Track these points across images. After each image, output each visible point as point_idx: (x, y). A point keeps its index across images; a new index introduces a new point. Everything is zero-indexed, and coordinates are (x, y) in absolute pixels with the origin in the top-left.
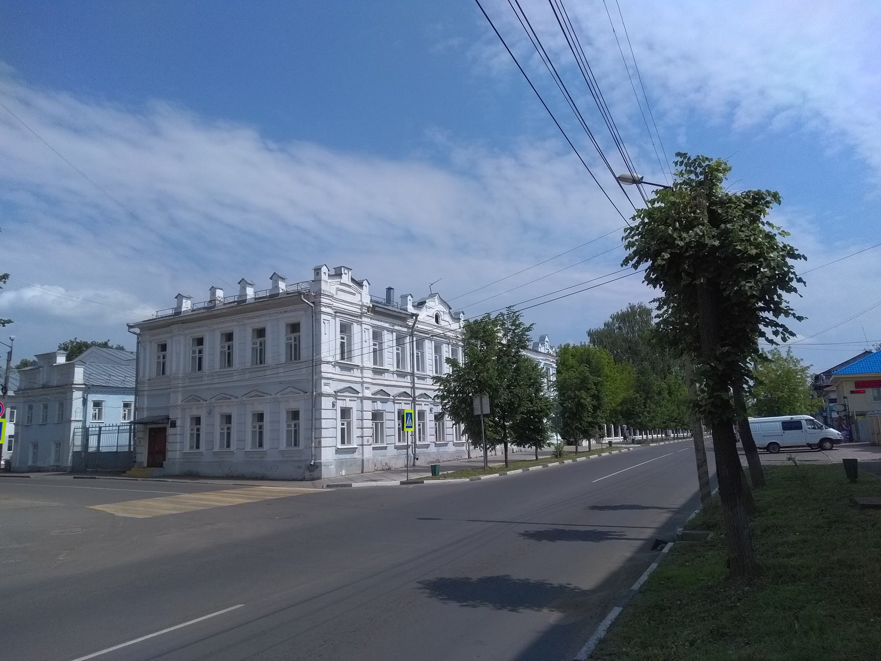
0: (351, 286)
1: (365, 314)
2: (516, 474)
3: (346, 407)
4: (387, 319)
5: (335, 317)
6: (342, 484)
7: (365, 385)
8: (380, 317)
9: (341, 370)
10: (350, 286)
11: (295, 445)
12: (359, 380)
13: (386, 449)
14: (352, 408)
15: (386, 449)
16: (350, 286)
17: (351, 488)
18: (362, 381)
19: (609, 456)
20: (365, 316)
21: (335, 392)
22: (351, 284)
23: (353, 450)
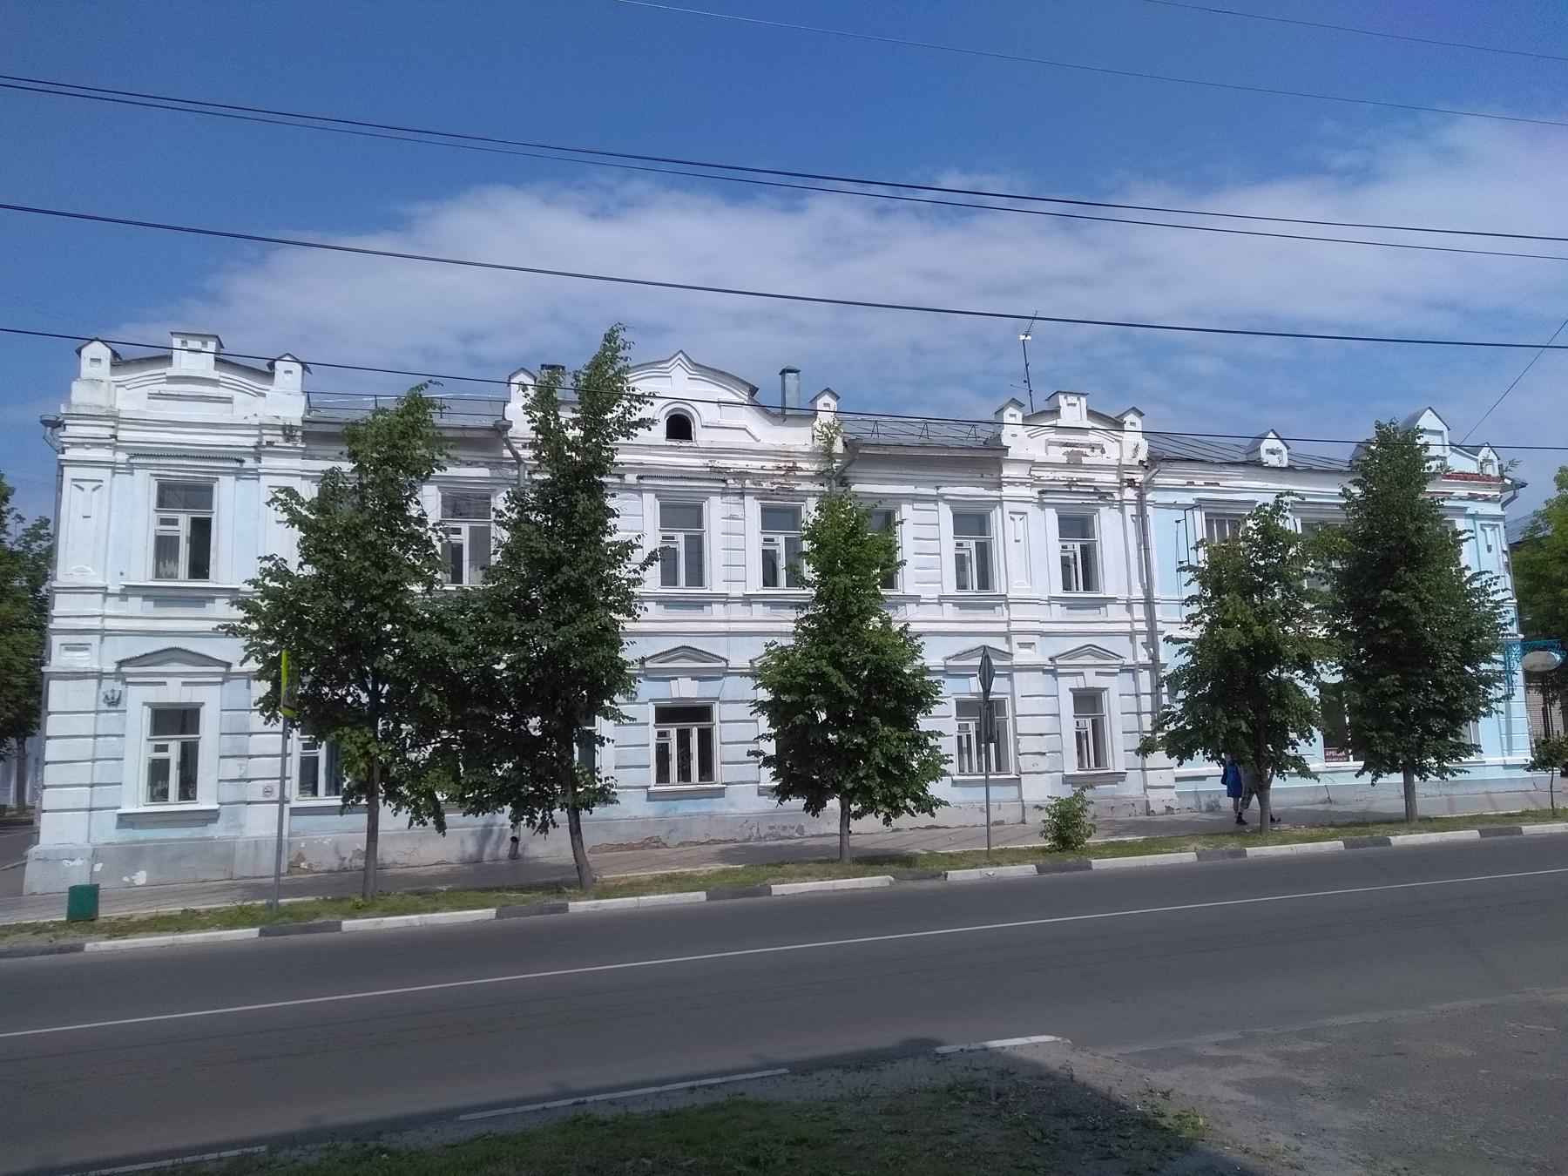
0: (219, 381)
1: (268, 449)
2: (189, 942)
3: (1086, 689)
4: (949, 474)
5: (1042, 505)
6: (547, 883)
7: (1015, 639)
8: (905, 473)
9: (155, 606)
10: (214, 382)
11: (1097, 764)
12: (1127, 627)
13: (1124, 780)
14: (203, 703)
15: (1124, 780)
16: (214, 382)
17: (1481, 827)
18: (1130, 630)
19: (570, 899)
20: (268, 452)
21: (1051, 659)
22: (1088, 424)
23: (210, 817)
